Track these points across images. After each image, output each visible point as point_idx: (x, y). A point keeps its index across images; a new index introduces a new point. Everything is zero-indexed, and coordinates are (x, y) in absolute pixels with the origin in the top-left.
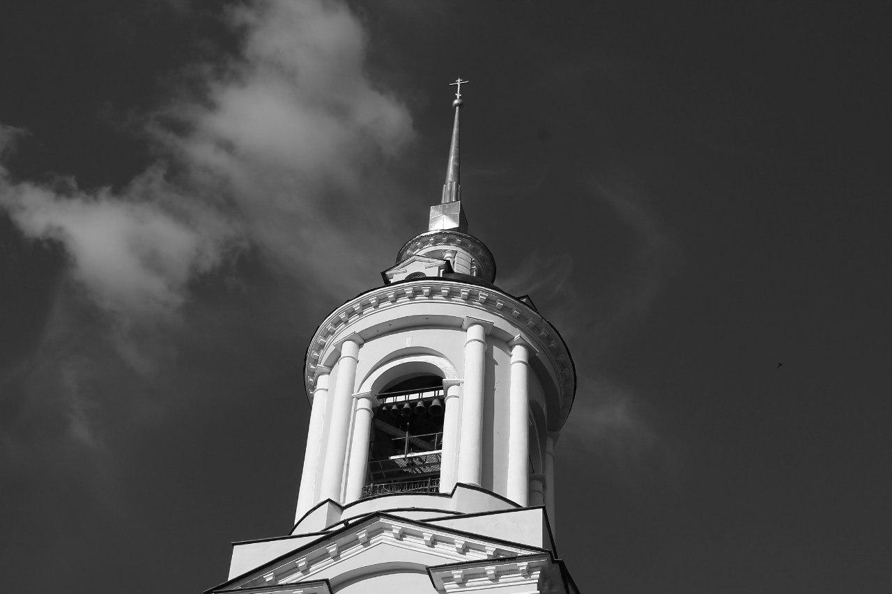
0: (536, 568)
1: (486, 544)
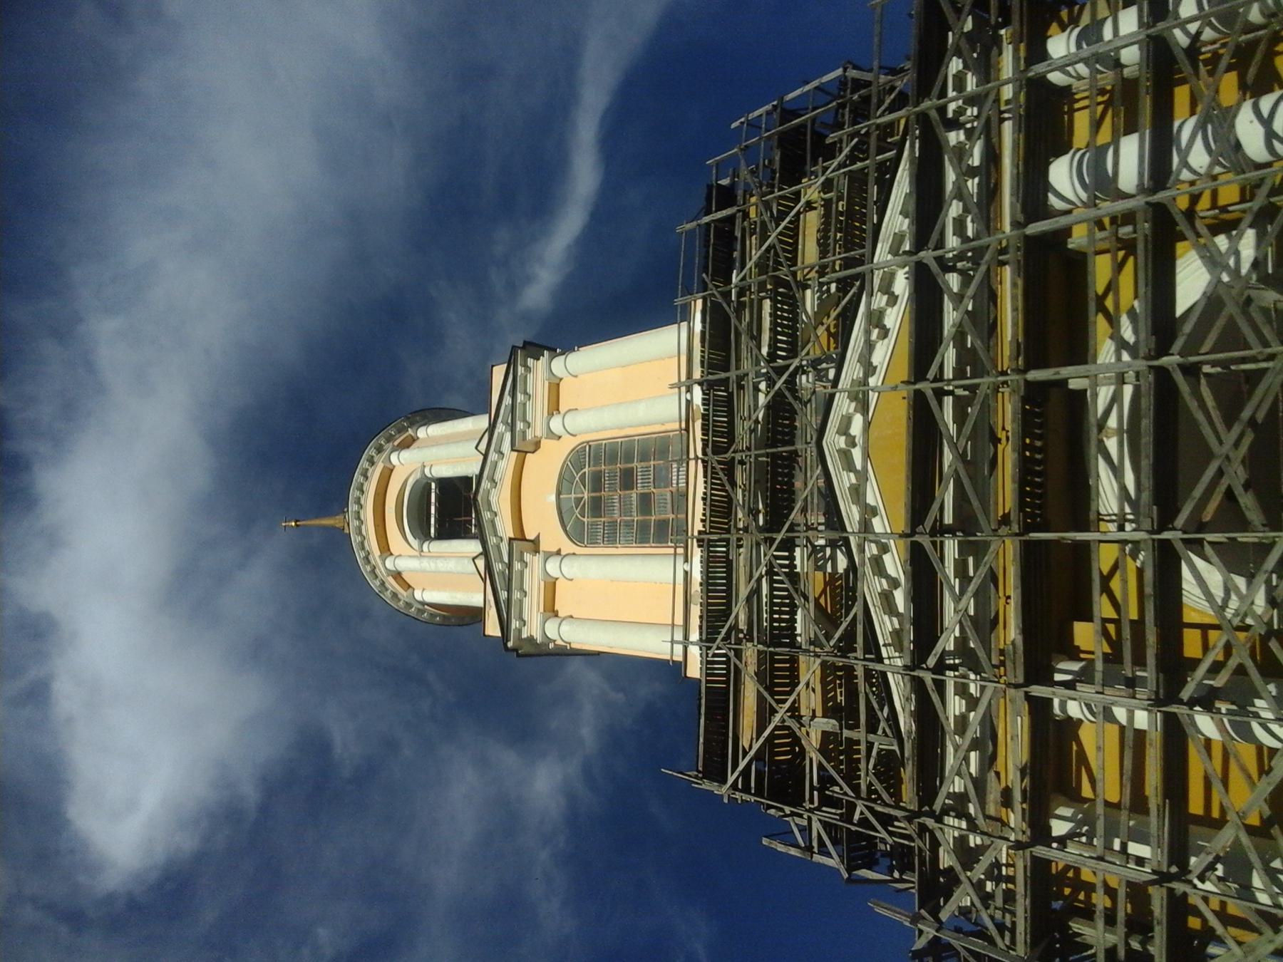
0: (526, 362)
1: (504, 403)
